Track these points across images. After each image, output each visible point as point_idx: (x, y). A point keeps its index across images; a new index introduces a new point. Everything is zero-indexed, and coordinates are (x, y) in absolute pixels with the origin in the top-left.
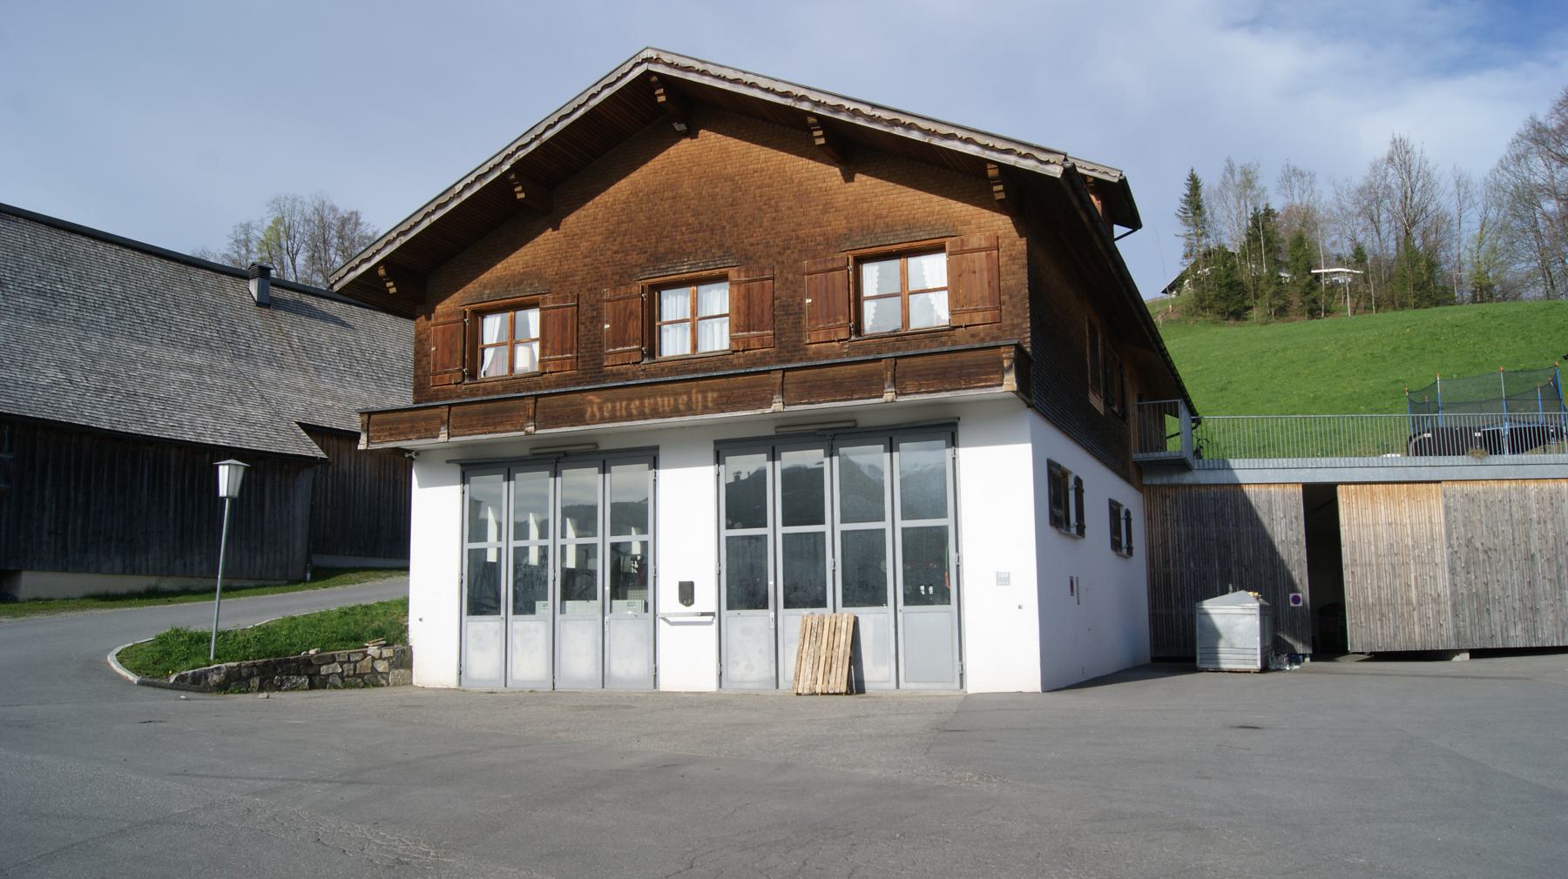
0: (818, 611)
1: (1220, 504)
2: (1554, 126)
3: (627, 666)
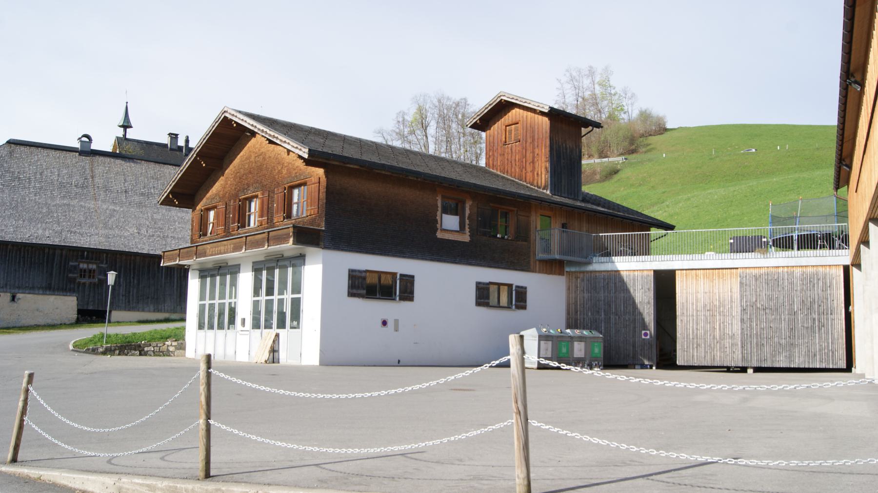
1: (606, 282)
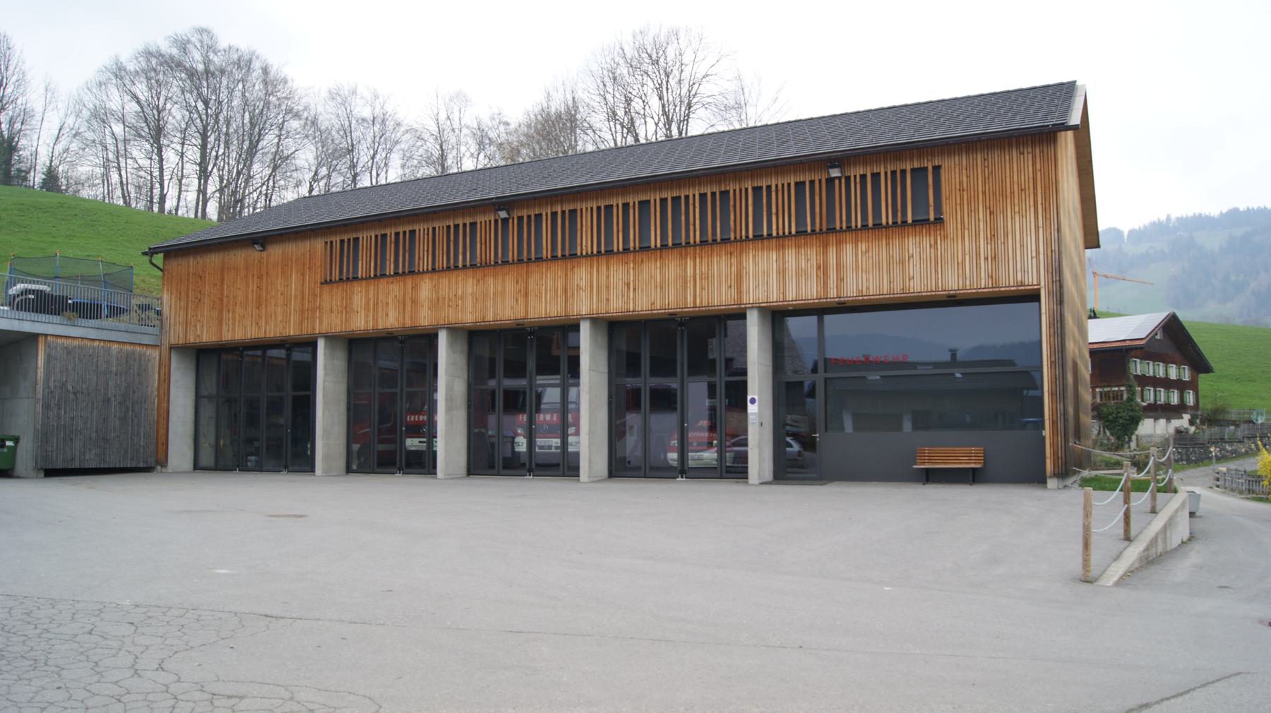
2: (132, 69)
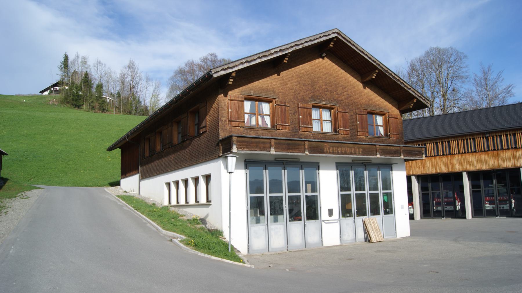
0: (365, 217)
3: (313, 239)
